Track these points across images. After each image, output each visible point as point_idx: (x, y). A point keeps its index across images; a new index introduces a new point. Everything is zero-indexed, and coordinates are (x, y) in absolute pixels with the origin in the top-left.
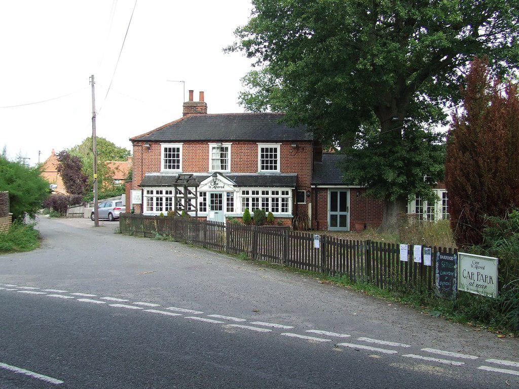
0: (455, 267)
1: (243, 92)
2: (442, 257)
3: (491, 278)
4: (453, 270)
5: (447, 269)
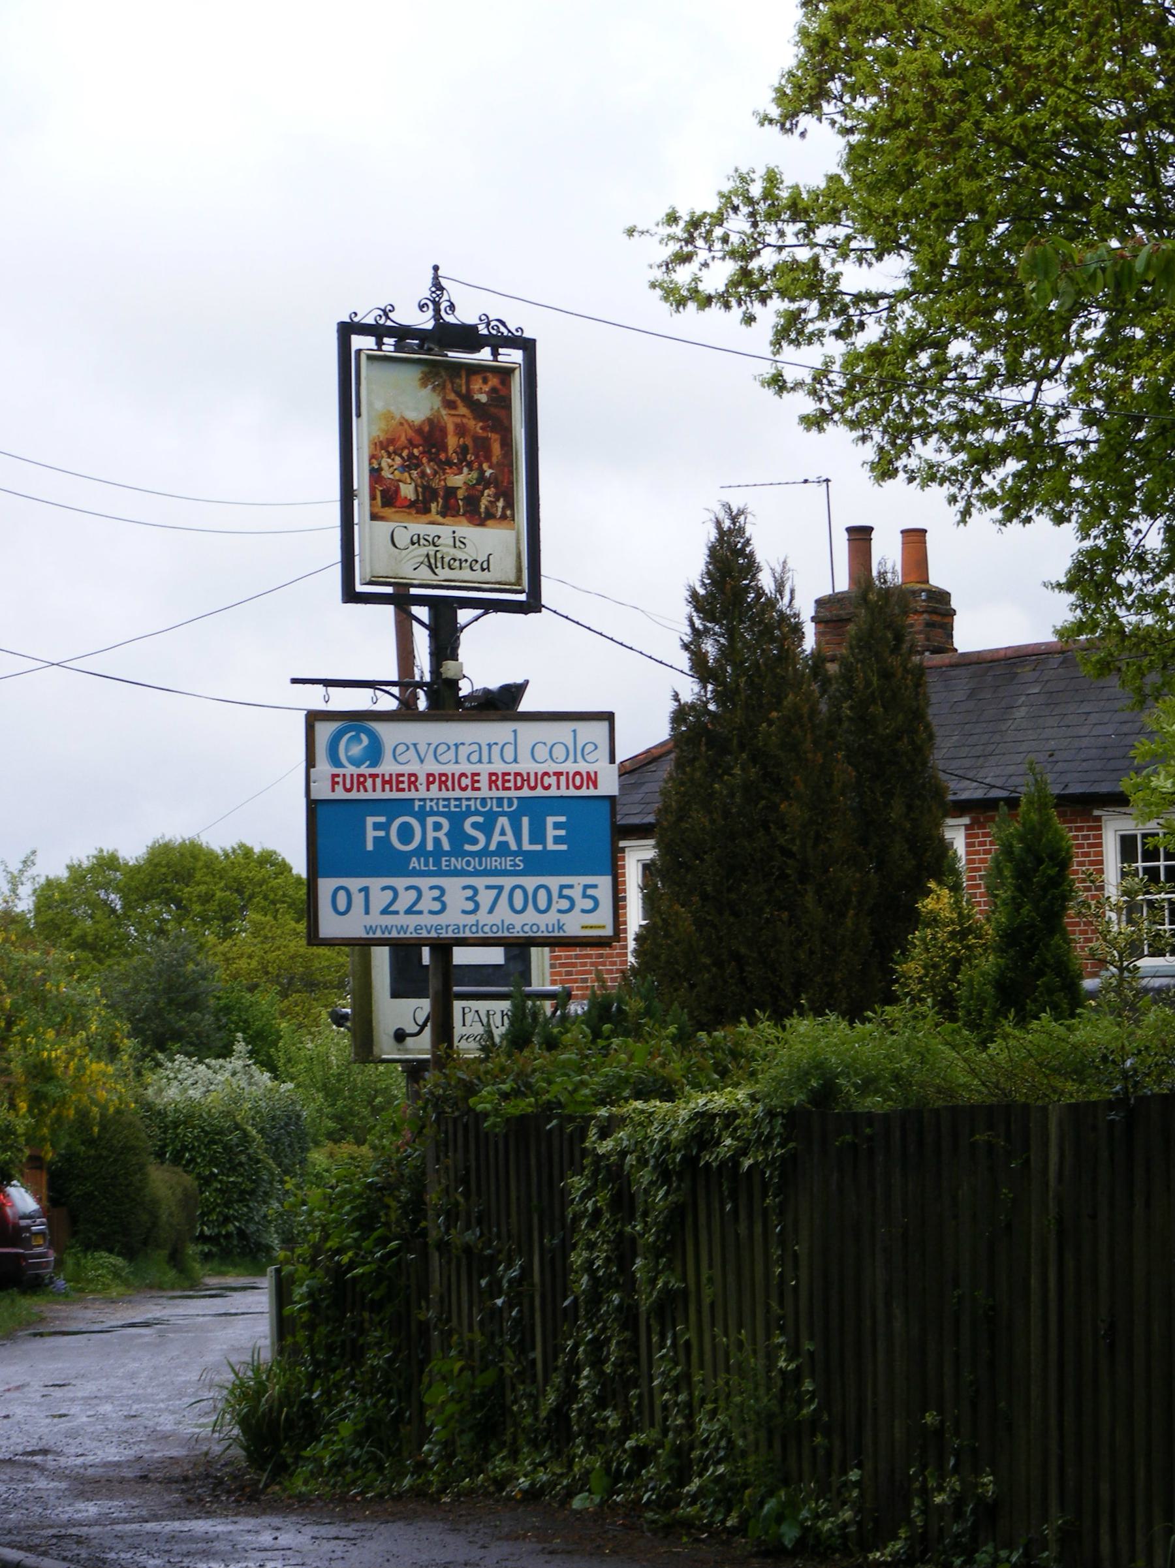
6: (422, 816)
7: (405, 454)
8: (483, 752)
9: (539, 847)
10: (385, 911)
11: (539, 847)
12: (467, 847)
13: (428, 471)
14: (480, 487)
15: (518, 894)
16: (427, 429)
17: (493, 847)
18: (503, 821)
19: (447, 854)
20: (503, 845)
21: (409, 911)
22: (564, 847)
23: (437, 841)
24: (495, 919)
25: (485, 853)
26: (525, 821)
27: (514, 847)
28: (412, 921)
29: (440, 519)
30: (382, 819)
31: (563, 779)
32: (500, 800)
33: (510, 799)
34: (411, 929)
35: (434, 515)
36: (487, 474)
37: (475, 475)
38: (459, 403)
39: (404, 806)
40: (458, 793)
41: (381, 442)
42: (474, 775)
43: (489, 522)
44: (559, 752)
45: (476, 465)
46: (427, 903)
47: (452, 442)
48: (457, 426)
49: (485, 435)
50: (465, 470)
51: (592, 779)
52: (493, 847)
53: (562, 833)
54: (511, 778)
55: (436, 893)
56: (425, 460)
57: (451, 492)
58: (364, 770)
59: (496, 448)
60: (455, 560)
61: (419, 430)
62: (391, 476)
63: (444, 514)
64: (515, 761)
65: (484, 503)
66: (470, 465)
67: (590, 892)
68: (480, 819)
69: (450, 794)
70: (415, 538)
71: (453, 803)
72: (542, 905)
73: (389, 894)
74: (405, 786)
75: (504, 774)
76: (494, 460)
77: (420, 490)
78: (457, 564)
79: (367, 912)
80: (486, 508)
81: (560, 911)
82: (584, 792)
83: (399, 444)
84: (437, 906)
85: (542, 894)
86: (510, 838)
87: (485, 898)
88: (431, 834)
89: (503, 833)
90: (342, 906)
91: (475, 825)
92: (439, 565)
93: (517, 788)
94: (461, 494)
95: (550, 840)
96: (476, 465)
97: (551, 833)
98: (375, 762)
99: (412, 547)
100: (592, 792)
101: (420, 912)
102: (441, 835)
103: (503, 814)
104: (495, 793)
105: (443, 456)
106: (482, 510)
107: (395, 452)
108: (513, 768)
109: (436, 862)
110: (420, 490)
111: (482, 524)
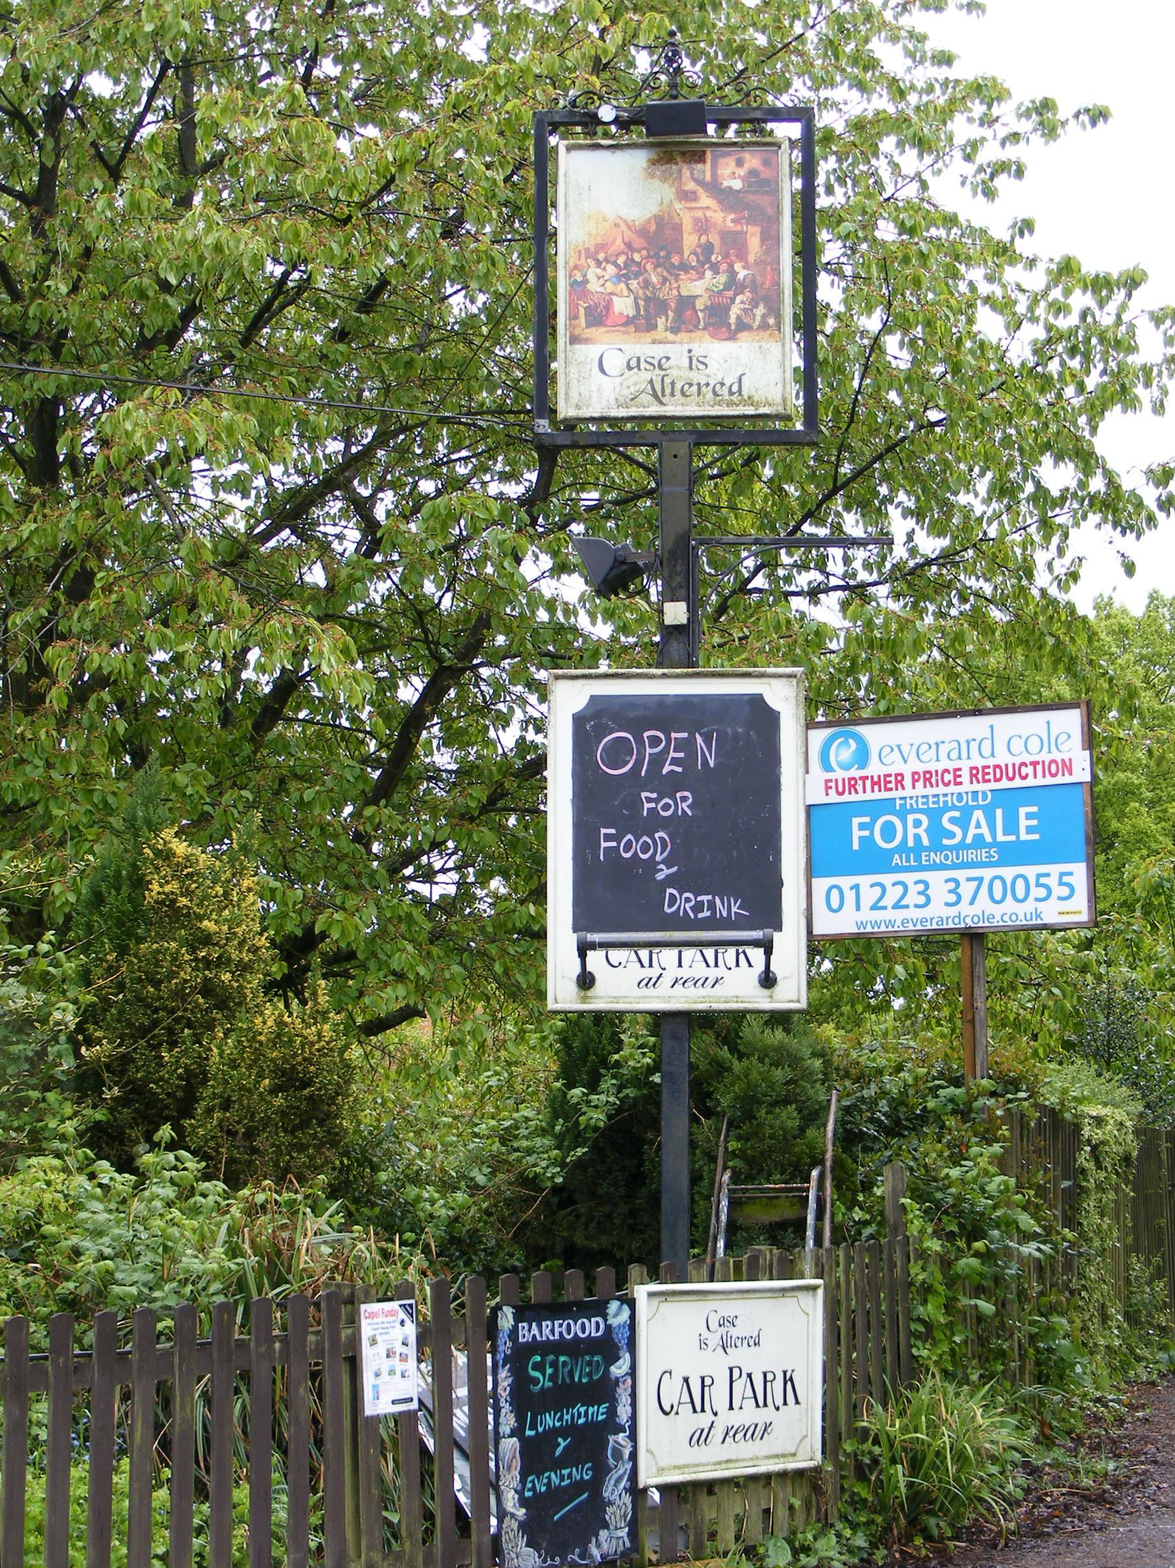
0: (619, 1369)
1: (1131, 536)
2: (528, 1333)
3: (788, 1380)
4: (603, 1391)
5: (564, 1395)
6: (902, 814)
7: (621, 260)
8: (962, 747)
9: (1013, 838)
10: (874, 907)
11: (1013, 838)
12: (945, 842)
13: (654, 279)
14: (730, 294)
15: (998, 884)
16: (653, 228)
17: (969, 840)
18: (978, 814)
19: (926, 849)
20: (979, 838)
21: (896, 906)
22: (1036, 837)
23: (917, 837)
24: (976, 910)
25: (962, 846)
26: (999, 813)
27: (988, 839)
28: (898, 916)
29: (671, 337)
30: (867, 819)
31: (1039, 768)
32: (975, 793)
33: (984, 793)
34: (898, 923)
35: (661, 332)
36: (741, 276)
37: (722, 278)
38: (701, 192)
39: (887, 806)
40: (941, 789)
41: (587, 250)
42: (956, 770)
43: (744, 335)
44: (1034, 745)
45: (724, 267)
46: (913, 898)
47: (690, 241)
48: (697, 221)
49: (739, 228)
50: (708, 274)
51: (1067, 767)
52: (969, 840)
53: (1034, 822)
54: (991, 770)
55: (921, 887)
56: (649, 267)
57: (686, 303)
58: (855, 773)
59: (754, 243)
60: (691, 385)
61: (643, 232)
62: (601, 289)
63: (675, 330)
64: (993, 755)
65: (735, 311)
66: (715, 268)
67: (1065, 879)
68: (957, 814)
69: (935, 791)
70: (633, 363)
71: (931, 799)
72: (1020, 894)
73: (878, 891)
74: (892, 785)
75: (984, 767)
76: (751, 258)
77: (641, 303)
78: (694, 389)
79: (858, 909)
80: (738, 318)
81: (1037, 900)
82: (1059, 780)
83: (613, 249)
84: (922, 900)
85: (1020, 883)
86: (985, 830)
87: (967, 890)
88: (911, 831)
89: (978, 826)
90: (835, 904)
91: (952, 820)
92: (668, 391)
93: (996, 780)
94: (700, 304)
95: (1022, 830)
96: (724, 267)
97: (1023, 823)
98: (863, 766)
99: (628, 373)
100: (1067, 779)
101: (907, 907)
102: (921, 831)
103: (978, 807)
104: (976, 787)
105: (675, 260)
106: (733, 320)
107: (607, 260)
108: (991, 762)
109: (915, 858)
110: (641, 303)
111: (732, 337)
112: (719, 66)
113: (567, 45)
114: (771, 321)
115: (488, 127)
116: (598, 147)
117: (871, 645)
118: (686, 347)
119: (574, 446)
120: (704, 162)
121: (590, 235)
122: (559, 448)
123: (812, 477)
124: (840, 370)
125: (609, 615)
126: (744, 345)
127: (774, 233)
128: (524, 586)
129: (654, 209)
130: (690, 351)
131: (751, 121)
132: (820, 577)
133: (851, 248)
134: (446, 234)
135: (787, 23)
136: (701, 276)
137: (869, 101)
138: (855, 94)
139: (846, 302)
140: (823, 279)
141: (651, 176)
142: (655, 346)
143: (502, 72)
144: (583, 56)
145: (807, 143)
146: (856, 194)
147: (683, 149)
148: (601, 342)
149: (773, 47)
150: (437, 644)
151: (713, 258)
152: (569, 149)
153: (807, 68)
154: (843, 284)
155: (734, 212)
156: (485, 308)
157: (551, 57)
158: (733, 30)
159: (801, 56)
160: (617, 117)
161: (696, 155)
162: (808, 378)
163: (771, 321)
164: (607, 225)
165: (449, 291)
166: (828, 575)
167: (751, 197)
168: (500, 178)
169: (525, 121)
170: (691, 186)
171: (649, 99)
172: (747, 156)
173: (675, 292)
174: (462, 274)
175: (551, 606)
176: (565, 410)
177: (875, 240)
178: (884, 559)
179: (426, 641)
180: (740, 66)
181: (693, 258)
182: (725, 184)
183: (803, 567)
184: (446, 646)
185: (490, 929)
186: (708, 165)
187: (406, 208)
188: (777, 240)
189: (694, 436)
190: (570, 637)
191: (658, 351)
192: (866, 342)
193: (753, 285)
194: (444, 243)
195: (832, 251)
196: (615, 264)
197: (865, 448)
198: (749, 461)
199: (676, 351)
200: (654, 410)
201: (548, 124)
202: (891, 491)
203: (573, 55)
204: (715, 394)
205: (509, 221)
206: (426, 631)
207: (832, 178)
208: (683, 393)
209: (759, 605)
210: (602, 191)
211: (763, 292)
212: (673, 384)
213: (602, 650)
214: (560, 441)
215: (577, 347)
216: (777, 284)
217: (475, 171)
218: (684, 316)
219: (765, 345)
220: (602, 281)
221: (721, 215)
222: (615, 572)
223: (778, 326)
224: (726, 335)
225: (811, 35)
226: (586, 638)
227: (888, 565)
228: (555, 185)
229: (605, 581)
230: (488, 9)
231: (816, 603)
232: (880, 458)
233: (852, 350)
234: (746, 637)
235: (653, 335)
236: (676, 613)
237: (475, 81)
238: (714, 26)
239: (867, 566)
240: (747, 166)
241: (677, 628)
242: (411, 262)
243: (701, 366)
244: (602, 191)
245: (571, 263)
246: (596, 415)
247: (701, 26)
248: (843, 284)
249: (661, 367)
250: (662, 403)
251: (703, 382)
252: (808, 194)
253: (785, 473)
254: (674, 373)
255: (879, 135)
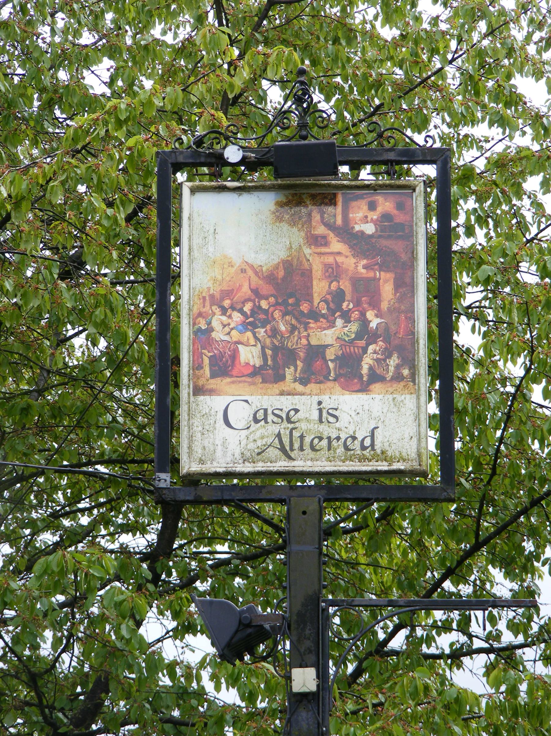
7: (247, 308)
13: (283, 328)
14: (362, 343)
29: (299, 388)
35: (289, 383)
37: (354, 327)
38: (331, 236)
41: (212, 296)
43: (376, 387)
45: (355, 315)
47: (320, 288)
48: (327, 267)
49: (371, 274)
50: (339, 322)
56: (277, 314)
57: (317, 352)
59: (387, 290)
60: (321, 439)
61: (270, 278)
62: (227, 338)
63: (304, 381)
65: (367, 362)
66: (346, 317)
70: (260, 415)
76: (384, 306)
77: (269, 352)
78: (324, 443)
80: (371, 368)
92: (296, 445)
94: (330, 354)
96: (355, 315)
99: (254, 426)
105: (305, 307)
106: (365, 370)
107: (233, 308)
110: (269, 352)
111: (364, 388)
112: (354, 102)
113: (192, 79)
114: (406, 372)
115: (109, 164)
116: (223, 189)
117: (515, 714)
118: (315, 399)
119: (197, 502)
120: (335, 204)
121: (215, 280)
122: (182, 504)
123: (453, 532)
124: (480, 419)
125: (233, 681)
126: (378, 397)
127: (407, 280)
128: (144, 646)
129: (283, 254)
130: (320, 403)
131: (385, 162)
132: (463, 639)
133: (493, 292)
134: (63, 276)
135: (425, 57)
136: (332, 325)
137: (511, 138)
138: (496, 132)
139: (485, 347)
140: (464, 324)
141: (279, 219)
142: (283, 398)
143: (123, 106)
144: (209, 90)
145: (443, 182)
146: (498, 235)
147: (313, 191)
148: (226, 394)
149: (411, 81)
150: (52, 708)
151: (345, 305)
152: (194, 191)
153: (445, 106)
154: (484, 329)
155: (366, 257)
156: (107, 353)
157: (174, 91)
158: (369, 64)
159: (440, 91)
160: (244, 158)
161: (327, 198)
162: (445, 424)
163: (406, 372)
164: (233, 270)
165: (71, 333)
166: (470, 636)
167: (385, 243)
168: (122, 216)
169: (148, 157)
170: (321, 230)
171: (277, 138)
172: (380, 199)
173: (304, 341)
174: (81, 316)
175: (171, 667)
176: (189, 465)
177: (517, 282)
178: (530, 619)
179: (40, 706)
180: (377, 102)
181: (323, 305)
182: (357, 228)
183: (446, 627)
184: (62, 710)
185: (461, 137)
186: (339, 208)
187: (22, 247)
188: (412, 288)
189: (323, 492)
190: (194, 702)
191: (286, 403)
192: (510, 389)
193: (384, 334)
194: (63, 285)
195: (473, 296)
196: (241, 311)
197: (508, 502)
198: (386, 515)
199: (306, 404)
200: (282, 465)
201: (170, 164)
202: (537, 547)
203: (199, 90)
204: (347, 448)
205: (132, 264)
206: (40, 695)
207: (473, 218)
208: (313, 448)
209: (396, 668)
210: (227, 234)
211: (397, 342)
212: (302, 437)
213: (228, 717)
214: (181, 496)
215: (201, 398)
216: (412, 333)
217: (94, 210)
218: (314, 368)
219: (399, 398)
220: (227, 329)
221: (353, 260)
222: (239, 636)
223: (413, 377)
224: (358, 387)
225: (450, 70)
226: (211, 703)
227: (535, 628)
228: (180, 225)
229: (229, 645)
230: (114, 40)
231: (459, 666)
232: (525, 511)
233: (493, 399)
234: (381, 704)
235: (282, 386)
236: (304, 679)
237: (94, 116)
238: (349, 60)
239: (513, 627)
240: (380, 209)
241: (304, 697)
242: (26, 304)
243: (331, 419)
244: (227, 234)
245: (195, 310)
246: (221, 470)
247: (335, 59)
248: (484, 329)
249: (289, 420)
250: (290, 458)
251: (334, 436)
252: (444, 237)
253: (425, 525)
254: (303, 426)
255: (523, 174)
